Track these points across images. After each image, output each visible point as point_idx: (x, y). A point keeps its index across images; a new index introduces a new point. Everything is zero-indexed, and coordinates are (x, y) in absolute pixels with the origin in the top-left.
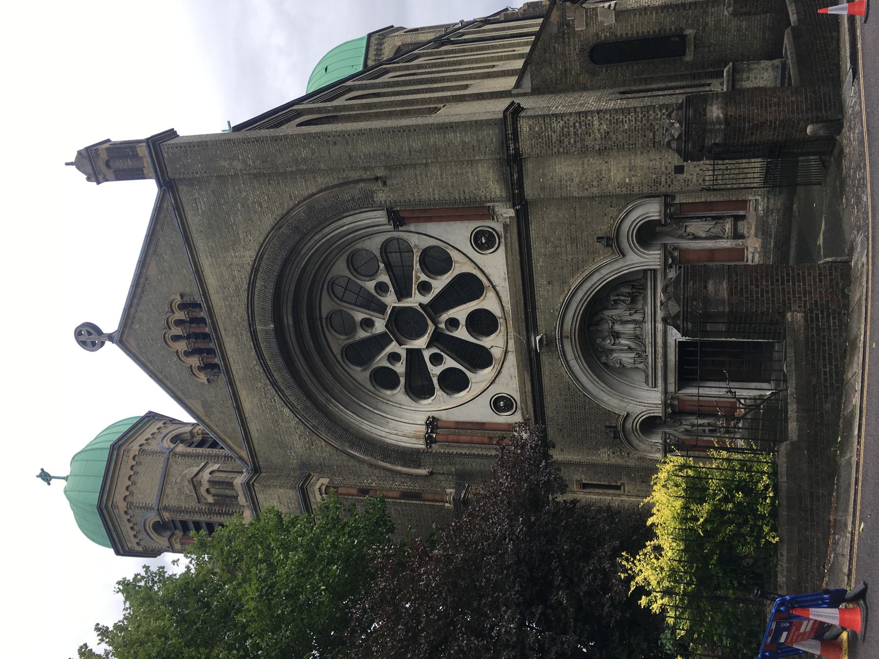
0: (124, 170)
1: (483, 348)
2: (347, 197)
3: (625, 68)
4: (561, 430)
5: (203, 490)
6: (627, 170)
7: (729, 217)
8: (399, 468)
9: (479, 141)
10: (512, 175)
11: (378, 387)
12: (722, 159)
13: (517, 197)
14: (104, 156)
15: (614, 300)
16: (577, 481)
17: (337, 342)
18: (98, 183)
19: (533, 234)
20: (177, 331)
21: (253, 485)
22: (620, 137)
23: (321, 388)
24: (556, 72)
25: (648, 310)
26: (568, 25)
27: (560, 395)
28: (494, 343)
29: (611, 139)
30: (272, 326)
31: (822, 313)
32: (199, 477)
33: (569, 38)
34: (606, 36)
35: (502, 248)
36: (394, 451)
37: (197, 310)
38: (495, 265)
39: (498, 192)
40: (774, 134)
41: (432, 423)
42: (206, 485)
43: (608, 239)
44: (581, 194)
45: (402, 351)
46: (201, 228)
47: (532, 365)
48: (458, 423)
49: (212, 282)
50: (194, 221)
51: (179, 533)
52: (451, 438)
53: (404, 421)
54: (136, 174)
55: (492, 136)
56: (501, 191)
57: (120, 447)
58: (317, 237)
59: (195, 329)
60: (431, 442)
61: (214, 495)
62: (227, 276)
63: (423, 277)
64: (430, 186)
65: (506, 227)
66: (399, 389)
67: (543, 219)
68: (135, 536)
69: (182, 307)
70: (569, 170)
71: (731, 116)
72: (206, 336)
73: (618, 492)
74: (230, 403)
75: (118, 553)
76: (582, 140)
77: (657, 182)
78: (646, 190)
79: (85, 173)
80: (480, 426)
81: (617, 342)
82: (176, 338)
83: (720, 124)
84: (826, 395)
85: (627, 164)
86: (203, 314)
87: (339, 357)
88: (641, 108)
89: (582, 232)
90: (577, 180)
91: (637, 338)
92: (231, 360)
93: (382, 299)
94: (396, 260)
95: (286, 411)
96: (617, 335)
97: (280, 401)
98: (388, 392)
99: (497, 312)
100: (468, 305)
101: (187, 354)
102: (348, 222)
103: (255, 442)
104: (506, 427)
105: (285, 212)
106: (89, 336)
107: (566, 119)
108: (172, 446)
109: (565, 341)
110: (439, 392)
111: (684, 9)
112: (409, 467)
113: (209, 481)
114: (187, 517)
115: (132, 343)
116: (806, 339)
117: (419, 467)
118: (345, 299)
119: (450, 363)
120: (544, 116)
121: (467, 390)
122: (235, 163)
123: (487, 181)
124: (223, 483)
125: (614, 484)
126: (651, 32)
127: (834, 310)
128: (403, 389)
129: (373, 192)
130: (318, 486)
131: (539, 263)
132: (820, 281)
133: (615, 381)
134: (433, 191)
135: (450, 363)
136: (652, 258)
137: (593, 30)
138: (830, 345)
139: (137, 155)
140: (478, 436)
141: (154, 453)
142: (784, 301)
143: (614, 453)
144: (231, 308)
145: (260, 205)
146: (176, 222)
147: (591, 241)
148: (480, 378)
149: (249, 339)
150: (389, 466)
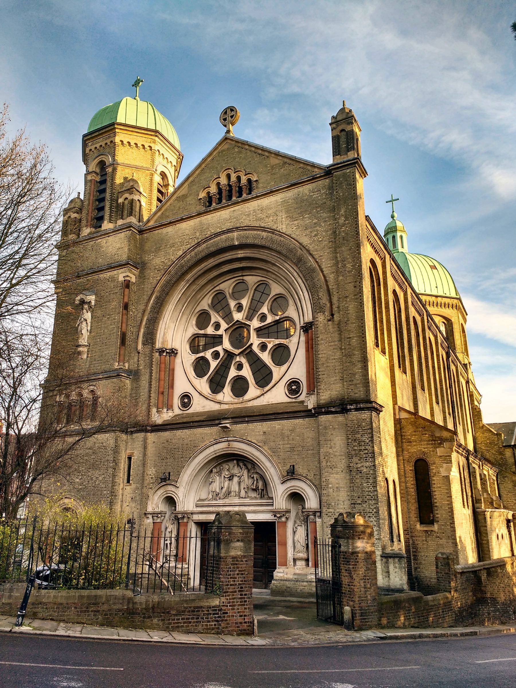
1: (223, 387)
2: (321, 294)
3: (412, 482)
4: (167, 441)
5: (127, 195)
6: (337, 485)
7: (308, 555)
8: (142, 330)
9: (356, 385)
10: (334, 407)
11: (197, 315)
12: (332, 550)
14: (348, 128)
15: (253, 477)
16: (133, 453)
17: (227, 286)
18: (330, 124)
19: (297, 421)
20: (233, 178)
21: (130, 230)
22: (358, 481)
23: (196, 276)
25: (247, 501)
26: (440, 444)
28: (226, 395)
31: (218, 617)
32: (136, 192)
33: (432, 444)
34: (433, 469)
35: (289, 400)
37: (248, 191)
38: (277, 395)
39: (322, 398)
41: (173, 353)
42: (130, 197)
43: (293, 473)
44: (322, 454)
46: (301, 195)
47: (211, 420)
48: (173, 370)
49: (265, 202)
51: (98, 179)
52: (163, 366)
53: (175, 331)
54: (337, 151)
55: (359, 393)
56: (325, 400)
57: (156, 136)
58: (295, 274)
59: (235, 190)
61: (123, 203)
63: (270, 346)
64: (327, 350)
65: (302, 402)
66: (197, 329)
67: (306, 428)
68: (96, 148)
69: (249, 181)
70: (338, 445)
71: (358, 556)
72: (230, 197)
73: (126, 481)
74: (185, 214)
75: (84, 136)
76: (356, 455)
77: (329, 506)
78: (324, 498)
79: (337, 115)
80: (171, 386)
81: (226, 479)
82: (229, 176)
83: (353, 549)
84: (163, 620)
85: (341, 486)
86: (244, 195)
87: (217, 288)
88: (377, 495)
89: (298, 455)
90: (331, 451)
91: (228, 494)
92: (214, 214)
93: (256, 318)
95: (180, 253)
96: (231, 478)
97: (187, 249)
98: (194, 322)
99: (247, 397)
100: (252, 377)
101: (218, 184)
102: (305, 296)
103: (160, 231)
104: (170, 403)
105: (311, 253)
107: (370, 443)
108: (158, 172)
109: (227, 443)
110: (194, 357)
111: (451, 523)
113: (132, 200)
114: (109, 184)
115: (225, 146)
116: (201, 607)
117: (144, 344)
118: (256, 292)
119: (214, 364)
120: (372, 429)
121: (196, 377)
123: (331, 390)
124: (132, 209)
125: (131, 479)
127: (220, 625)
130: (130, 274)
131: (277, 425)
132: (241, 616)
133: (201, 478)
134: (324, 353)
135: (214, 364)
136: (281, 502)
137: (438, 461)
138: (197, 622)
140: (165, 384)
141: (153, 161)
142: (228, 592)
143: (152, 478)
144: (248, 215)
145: (316, 235)
146: (305, 178)
147: (291, 461)
149: (228, 228)
150: (144, 323)
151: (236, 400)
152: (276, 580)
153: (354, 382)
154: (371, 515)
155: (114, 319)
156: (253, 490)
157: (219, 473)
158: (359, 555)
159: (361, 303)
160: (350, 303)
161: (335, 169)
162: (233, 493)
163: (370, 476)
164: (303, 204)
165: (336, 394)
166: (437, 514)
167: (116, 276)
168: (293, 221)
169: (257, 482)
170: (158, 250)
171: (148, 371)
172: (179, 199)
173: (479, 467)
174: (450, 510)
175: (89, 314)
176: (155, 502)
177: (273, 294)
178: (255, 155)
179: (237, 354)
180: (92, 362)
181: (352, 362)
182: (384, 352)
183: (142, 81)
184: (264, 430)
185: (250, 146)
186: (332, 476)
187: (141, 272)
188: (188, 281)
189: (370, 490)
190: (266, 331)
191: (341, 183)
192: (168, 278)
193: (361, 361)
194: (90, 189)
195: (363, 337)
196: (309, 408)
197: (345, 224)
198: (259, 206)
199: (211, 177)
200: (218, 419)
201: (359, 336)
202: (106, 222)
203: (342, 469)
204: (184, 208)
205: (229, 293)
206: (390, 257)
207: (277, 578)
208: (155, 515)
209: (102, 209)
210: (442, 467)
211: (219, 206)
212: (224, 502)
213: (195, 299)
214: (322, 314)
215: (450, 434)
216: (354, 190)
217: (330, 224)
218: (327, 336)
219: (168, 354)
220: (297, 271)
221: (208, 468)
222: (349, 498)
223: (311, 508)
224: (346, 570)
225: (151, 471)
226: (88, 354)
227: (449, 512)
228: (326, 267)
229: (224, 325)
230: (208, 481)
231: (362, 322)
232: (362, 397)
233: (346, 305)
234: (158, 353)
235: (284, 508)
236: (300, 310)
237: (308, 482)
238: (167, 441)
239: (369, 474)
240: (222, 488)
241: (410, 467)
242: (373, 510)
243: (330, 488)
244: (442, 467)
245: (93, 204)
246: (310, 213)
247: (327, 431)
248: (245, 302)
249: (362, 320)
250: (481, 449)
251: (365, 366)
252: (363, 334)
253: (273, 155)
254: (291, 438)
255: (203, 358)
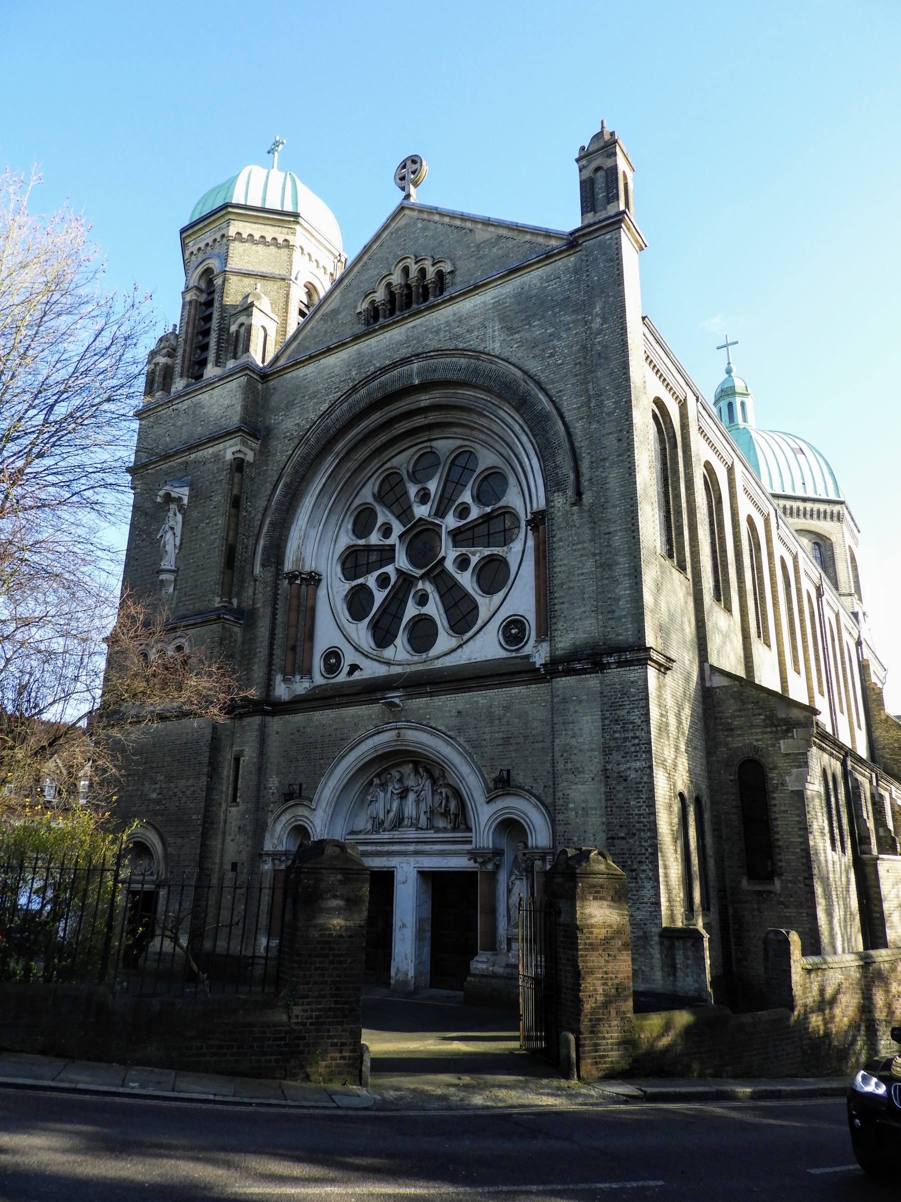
0: (592, 188)
1: (396, 637)
2: (559, 459)
3: (734, 803)
4: (298, 731)
6: (584, 805)
8: (262, 542)
9: (619, 618)
10: (579, 661)
13: (559, 666)
16: (242, 751)
18: (577, 160)
22: (620, 795)
24: (729, 718)
26: (788, 730)
27: (336, 729)
28: (399, 650)
29: (618, 783)
30: (417, 382)
33: (771, 732)
34: (772, 779)
36: (281, 535)
38: (486, 646)
40: (567, 989)
41: (314, 579)
44: (557, 749)
45: (393, 539)
47: (372, 690)
49: (467, 305)
50: (533, 277)
51: (203, 298)
55: (626, 635)
56: (562, 649)
58: (517, 428)
60: (290, 578)
61: (238, 332)
62: (469, 319)
63: (474, 560)
65: (528, 657)
66: (354, 538)
69: (440, 274)
73: (230, 799)
75: (182, 231)
76: (618, 748)
82: (406, 271)
85: (592, 805)
90: (573, 742)
91: (399, 822)
92: (381, 337)
93: (451, 512)
94: (495, 526)
95: (326, 406)
96: (403, 795)
98: (350, 526)
99: (434, 652)
100: (444, 616)
103: (294, 374)
106: (409, 170)
111: (805, 878)
112: (263, 554)
117: (263, 565)
119: (379, 596)
121: (350, 619)
122: (598, 320)
123: (578, 629)
125: (239, 794)
126: (777, 837)
128: (352, 543)
129: (564, 491)
131: (481, 698)
134: (564, 565)
135: (379, 596)
137: (782, 763)
139: (609, 203)
142: (306, 997)
143: (273, 794)
144: (437, 332)
147: (505, 762)
148: (361, 632)
150: (265, 530)
151: (416, 658)
152: (474, 975)
153: (616, 615)
154: (644, 860)
155: (216, 524)
156: (442, 814)
157: (383, 786)
158: (595, 931)
159: (630, 468)
160: (610, 470)
161: (584, 235)
162: (406, 820)
163: (643, 787)
164: (531, 303)
165: (585, 638)
166: (781, 861)
167: (221, 453)
168: (512, 334)
169: (447, 801)
170: (290, 405)
171: (269, 610)
172: (324, 318)
173: (871, 782)
174: (804, 854)
175: (179, 517)
176: (277, 835)
177: (481, 468)
178: (450, 230)
179: (417, 576)
180: (180, 598)
181: (613, 577)
182: (682, 568)
183: (283, 143)
184: (460, 707)
185: (441, 214)
186: (574, 787)
187: (262, 445)
188: (338, 453)
189: (642, 812)
190: (469, 534)
191: (596, 259)
192: (305, 451)
193: (629, 575)
194: (189, 316)
195: (633, 531)
196: (537, 666)
197: (602, 330)
198: (455, 314)
199: (378, 275)
200: (380, 690)
201: (627, 529)
202: (210, 366)
203: (592, 775)
204: (333, 331)
205: (408, 472)
206: (697, 400)
207: (477, 972)
208: (278, 857)
209: (205, 347)
210: (789, 774)
211: (390, 320)
212: (391, 836)
213: (350, 487)
214: (561, 494)
215: (808, 714)
216: (618, 270)
217: (576, 333)
218: (569, 533)
219: (304, 582)
220: (521, 422)
221: (365, 777)
222: (604, 827)
223: (537, 848)
224: (568, 960)
225: (273, 783)
226: (175, 585)
227: (803, 857)
228: (569, 410)
229: (398, 528)
230: (363, 800)
231: (631, 502)
232: (631, 640)
233: (603, 475)
234: (287, 581)
235: (491, 846)
236: (526, 494)
237: (533, 800)
238: (298, 731)
239: (640, 783)
240: (389, 812)
241: (731, 775)
242: (647, 850)
243: (572, 810)
244: (789, 774)
245: (192, 340)
246: (543, 317)
247: (567, 706)
248: (433, 486)
249: (632, 499)
250: (884, 758)
251: (636, 584)
252: (633, 525)
253: (480, 226)
254: (505, 720)
255: (363, 587)
